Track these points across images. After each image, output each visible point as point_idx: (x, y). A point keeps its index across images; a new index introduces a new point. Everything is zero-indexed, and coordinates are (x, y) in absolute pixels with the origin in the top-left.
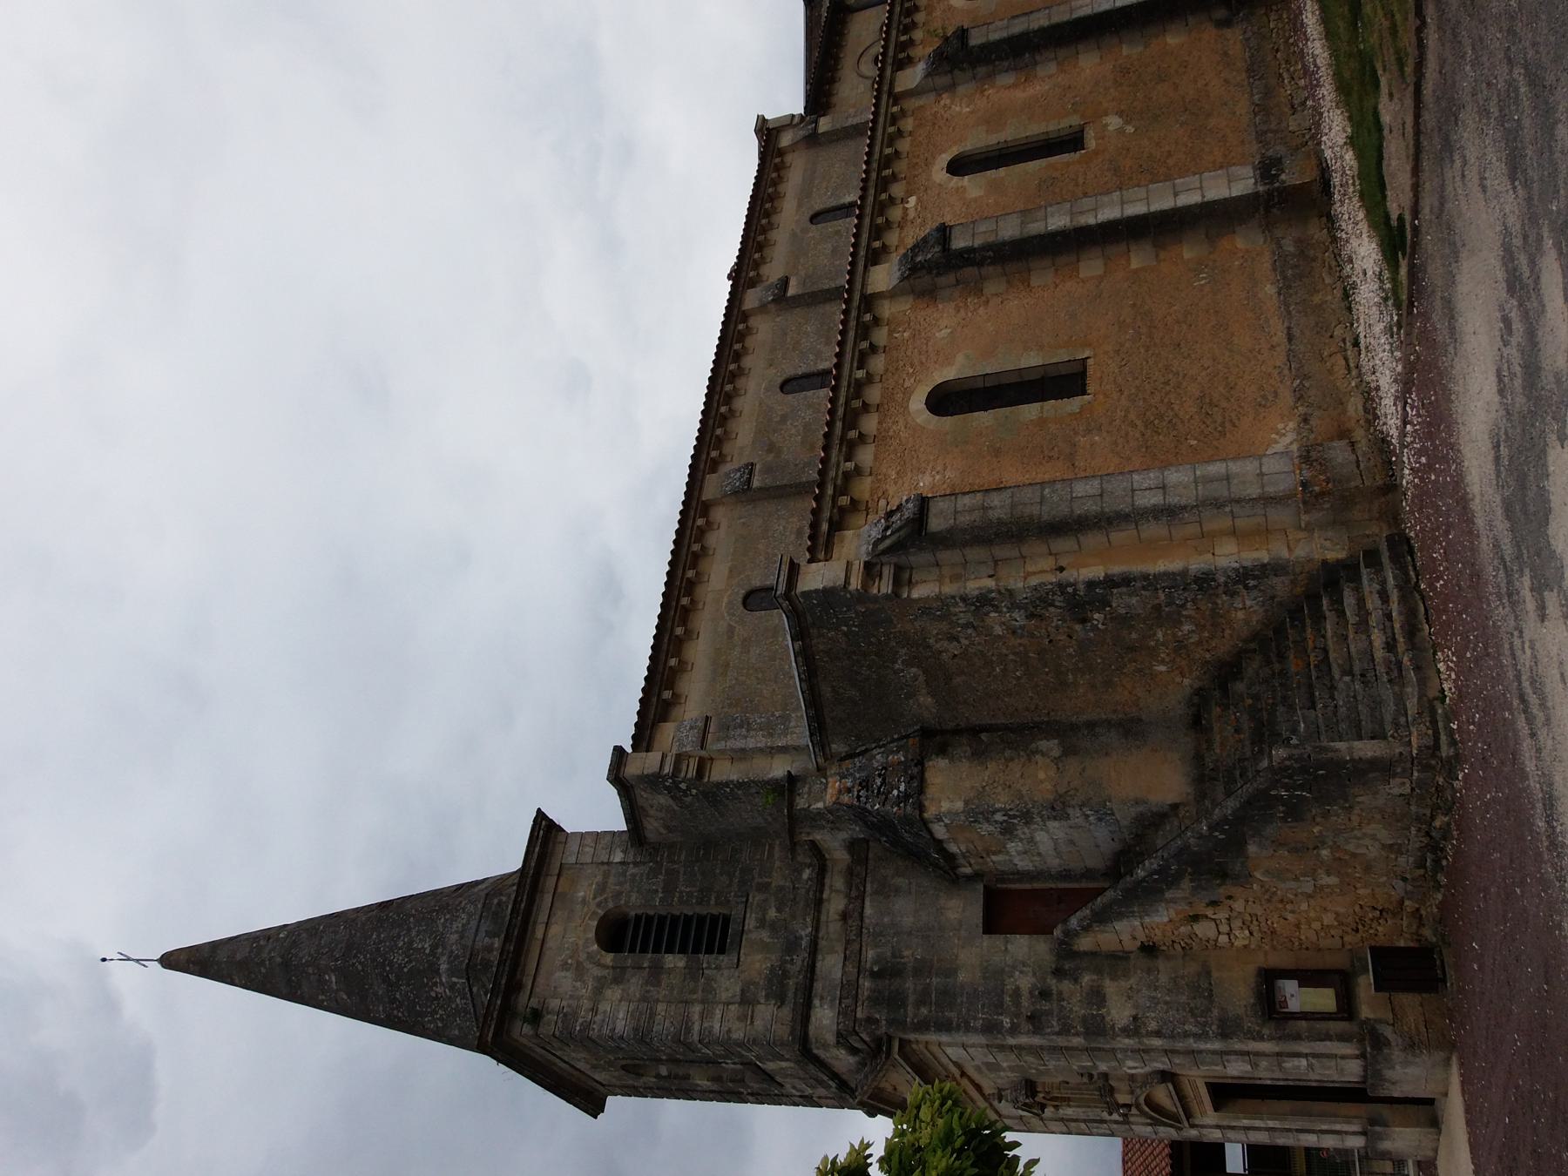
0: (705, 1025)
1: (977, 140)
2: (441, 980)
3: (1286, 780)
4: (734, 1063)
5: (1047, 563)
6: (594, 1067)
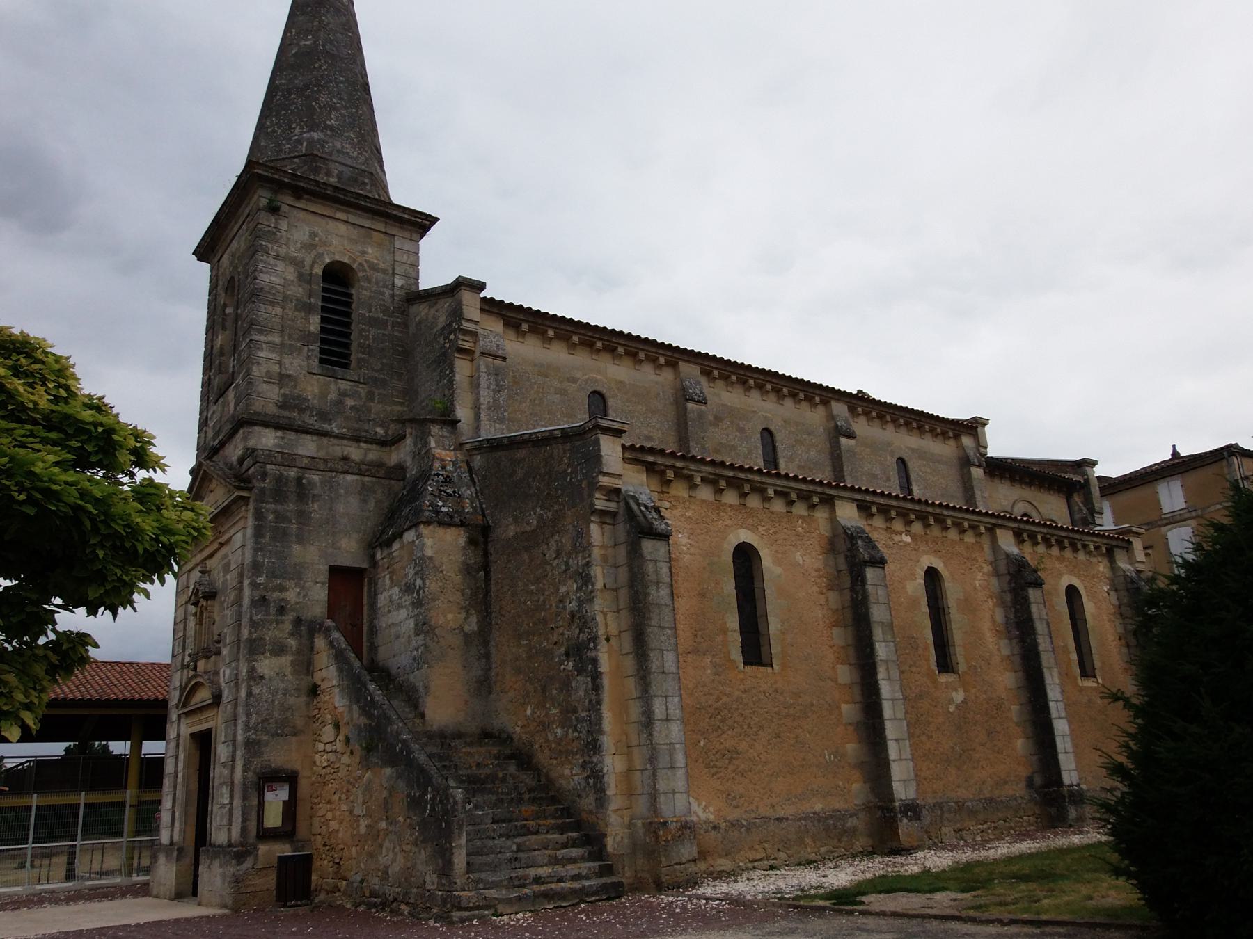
0: (264, 346)
1: (952, 592)
2: (305, 133)
4: (233, 366)
5: (613, 630)
6: (233, 255)
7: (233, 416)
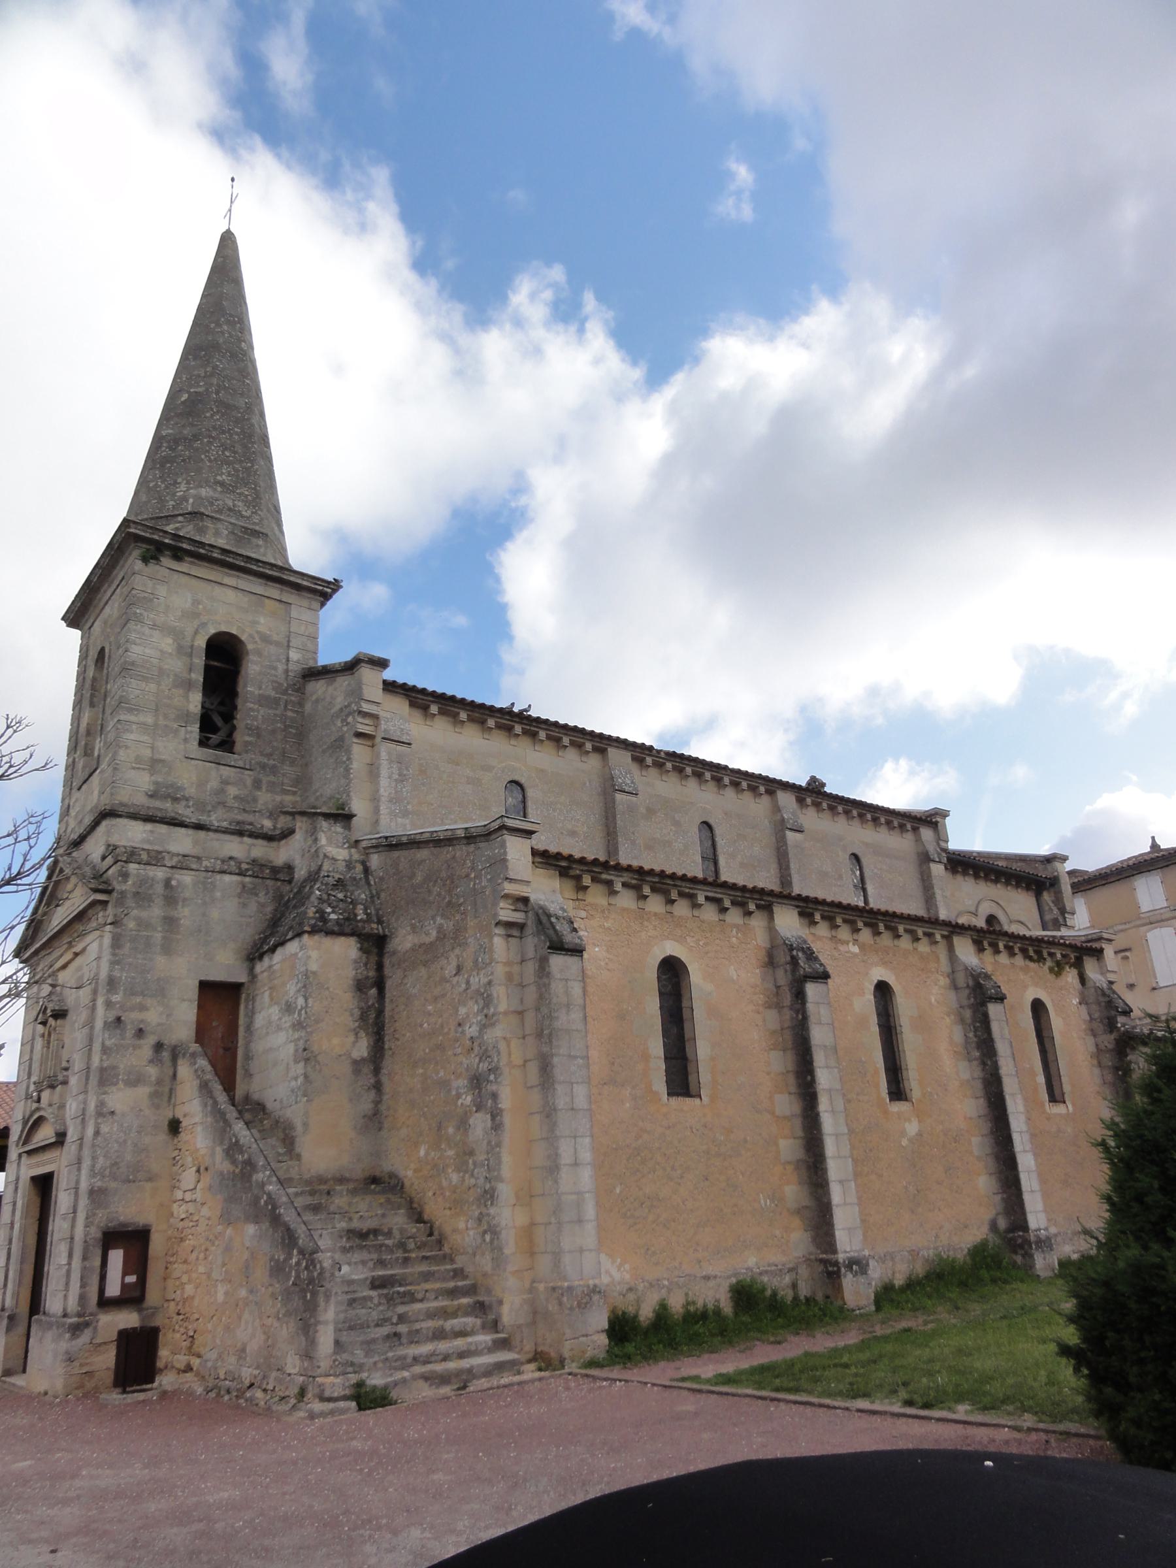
0: (134, 726)
1: (904, 1008)
2: (192, 488)
3: (304, 1264)
4: (99, 750)
5: (517, 1058)
6: (105, 623)
7: (96, 807)
